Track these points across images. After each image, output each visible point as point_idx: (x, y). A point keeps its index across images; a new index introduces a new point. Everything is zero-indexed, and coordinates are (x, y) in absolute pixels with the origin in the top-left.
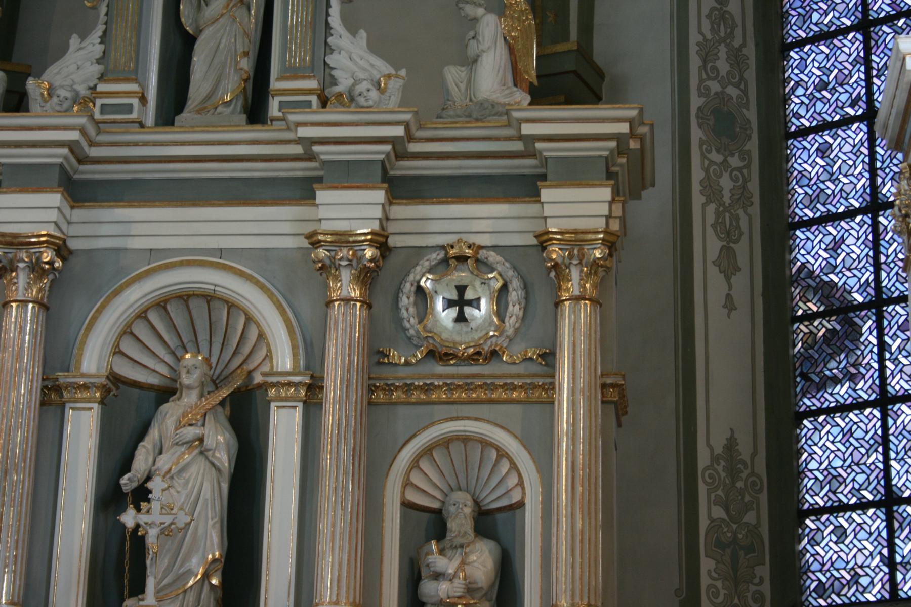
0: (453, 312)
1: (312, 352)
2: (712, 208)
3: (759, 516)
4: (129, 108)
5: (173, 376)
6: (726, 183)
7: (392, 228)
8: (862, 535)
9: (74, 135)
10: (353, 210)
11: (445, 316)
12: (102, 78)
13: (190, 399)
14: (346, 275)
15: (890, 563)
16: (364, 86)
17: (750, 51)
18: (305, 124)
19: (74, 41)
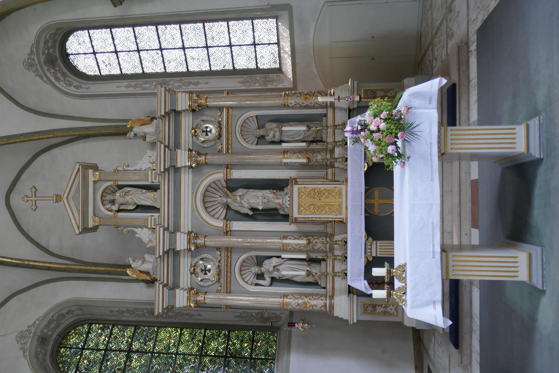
1: (219, 166)
2: (183, 87)
3: (258, 77)
4: (155, 219)
6: (177, 84)
7: (186, 288)
8: (262, 51)
10: (183, 159)
12: (147, 227)
13: (229, 200)
15: (269, 44)
17: (144, 80)
18: (160, 169)
19: (137, 236)
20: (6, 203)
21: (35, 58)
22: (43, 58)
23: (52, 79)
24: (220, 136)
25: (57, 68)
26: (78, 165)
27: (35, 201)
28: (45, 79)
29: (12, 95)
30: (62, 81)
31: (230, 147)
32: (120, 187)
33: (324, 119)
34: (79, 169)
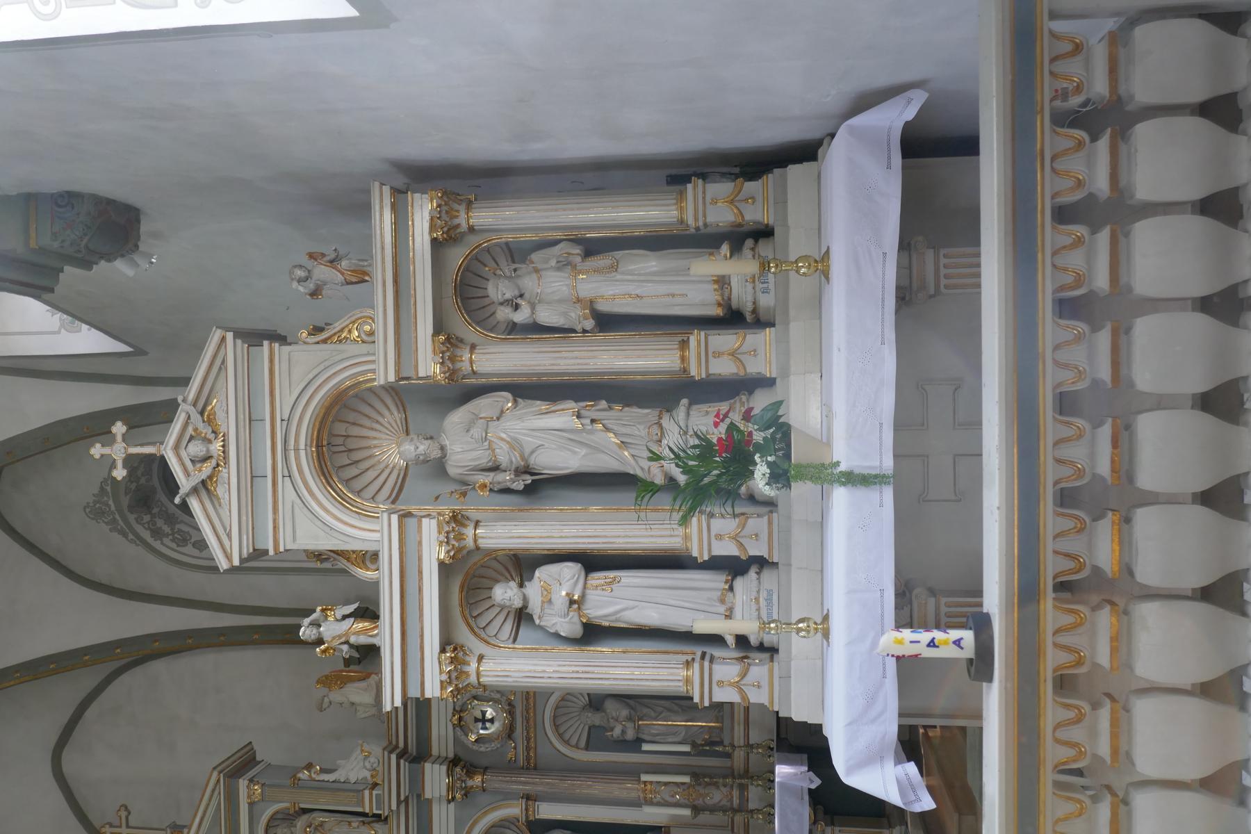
0: (488, 725)
5: (492, 321)
9: (394, 757)
10: (436, 779)
11: (492, 729)
14: (470, 783)
16: (367, 765)
20: (55, 775)
21: (111, 502)
22: (125, 501)
23: (146, 535)
24: (510, 732)
25: (155, 510)
26: (215, 774)
27: (128, 826)
28: (131, 536)
29: (59, 558)
30: (168, 535)
31: (532, 754)
32: (305, 811)
33: (722, 609)
34: (218, 781)
